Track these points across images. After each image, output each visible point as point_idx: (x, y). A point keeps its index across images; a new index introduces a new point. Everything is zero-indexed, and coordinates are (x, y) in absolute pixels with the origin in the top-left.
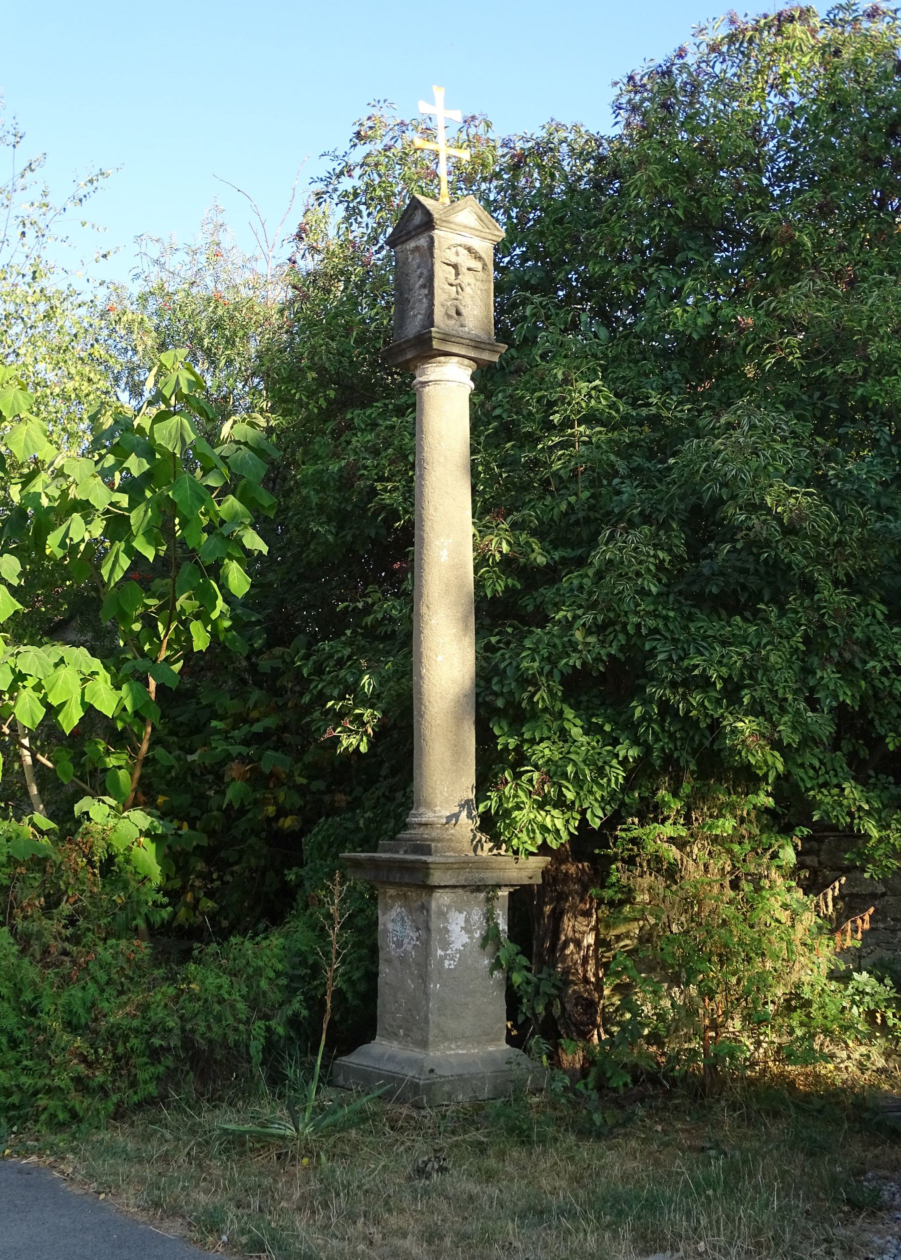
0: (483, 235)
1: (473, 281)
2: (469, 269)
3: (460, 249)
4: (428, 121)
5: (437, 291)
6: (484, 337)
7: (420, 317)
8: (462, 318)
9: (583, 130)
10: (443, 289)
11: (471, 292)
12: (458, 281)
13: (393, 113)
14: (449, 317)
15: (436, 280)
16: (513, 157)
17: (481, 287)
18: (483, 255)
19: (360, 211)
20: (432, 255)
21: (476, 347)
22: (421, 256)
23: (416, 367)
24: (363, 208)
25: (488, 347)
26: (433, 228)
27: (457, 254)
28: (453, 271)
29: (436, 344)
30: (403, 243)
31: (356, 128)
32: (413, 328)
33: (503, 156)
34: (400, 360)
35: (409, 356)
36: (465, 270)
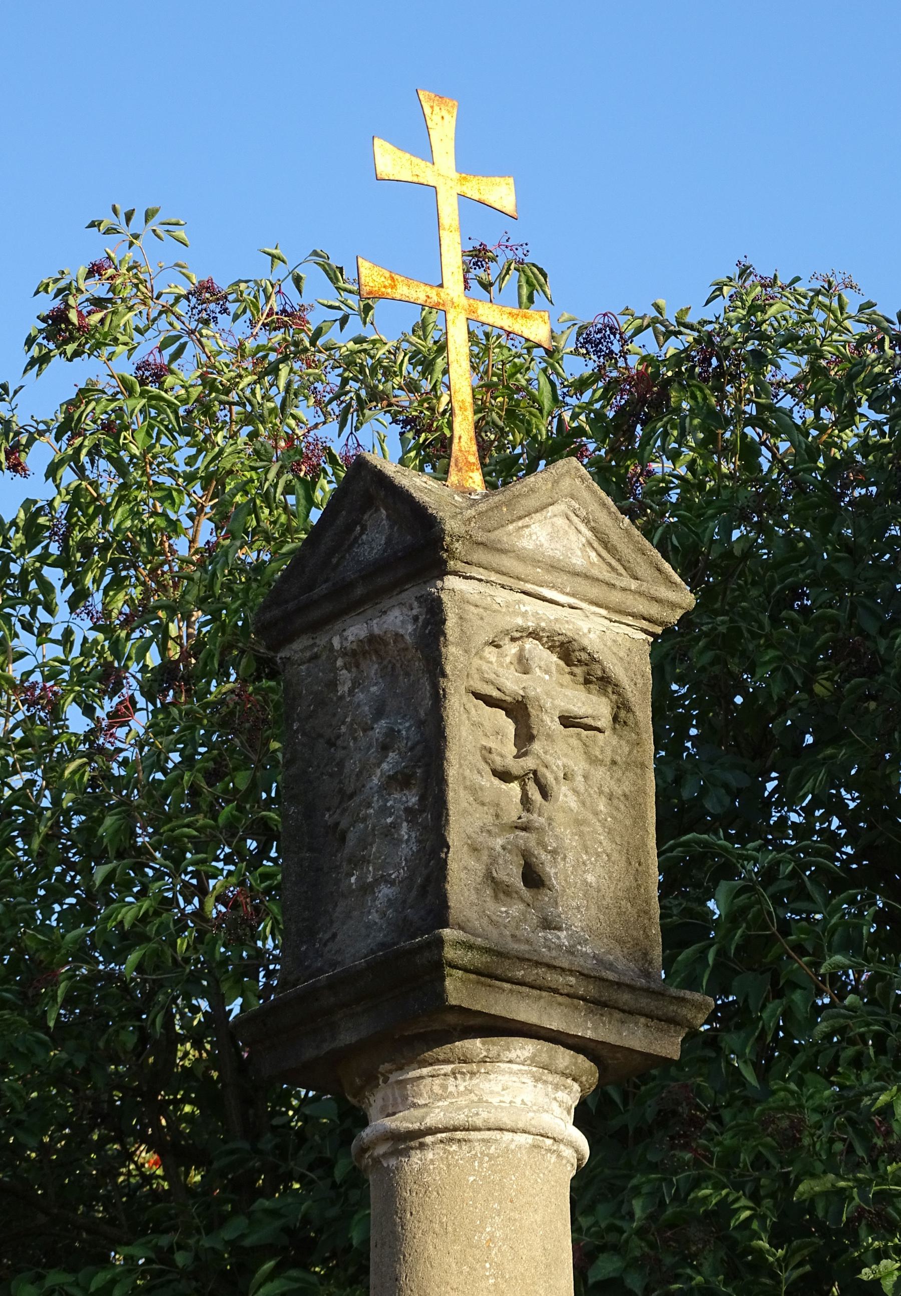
0: (615, 597)
1: (579, 766)
2: (567, 721)
3: (530, 644)
4: (289, 287)
5: (458, 799)
6: (624, 966)
7: (385, 892)
8: (545, 897)
9: (852, 303)
10: (474, 790)
11: (572, 802)
12: (529, 763)
13: (170, 252)
14: (500, 890)
15: (452, 755)
16: (612, 387)
17: (610, 785)
18: (618, 672)
19: (46, 587)
20: (435, 668)
21: (598, 1005)
22: (389, 673)
23: (371, 1080)
24: (54, 575)
25: (644, 1002)
26: (442, 571)
27: (523, 664)
28: (510, 727)
29: (457, 990)
30: (316, 627)
31: (48, 304)
32: (364, 925)
33: (581, 385)
34: (309, 1053)
35: (347, 1038)
36: (556, 726)
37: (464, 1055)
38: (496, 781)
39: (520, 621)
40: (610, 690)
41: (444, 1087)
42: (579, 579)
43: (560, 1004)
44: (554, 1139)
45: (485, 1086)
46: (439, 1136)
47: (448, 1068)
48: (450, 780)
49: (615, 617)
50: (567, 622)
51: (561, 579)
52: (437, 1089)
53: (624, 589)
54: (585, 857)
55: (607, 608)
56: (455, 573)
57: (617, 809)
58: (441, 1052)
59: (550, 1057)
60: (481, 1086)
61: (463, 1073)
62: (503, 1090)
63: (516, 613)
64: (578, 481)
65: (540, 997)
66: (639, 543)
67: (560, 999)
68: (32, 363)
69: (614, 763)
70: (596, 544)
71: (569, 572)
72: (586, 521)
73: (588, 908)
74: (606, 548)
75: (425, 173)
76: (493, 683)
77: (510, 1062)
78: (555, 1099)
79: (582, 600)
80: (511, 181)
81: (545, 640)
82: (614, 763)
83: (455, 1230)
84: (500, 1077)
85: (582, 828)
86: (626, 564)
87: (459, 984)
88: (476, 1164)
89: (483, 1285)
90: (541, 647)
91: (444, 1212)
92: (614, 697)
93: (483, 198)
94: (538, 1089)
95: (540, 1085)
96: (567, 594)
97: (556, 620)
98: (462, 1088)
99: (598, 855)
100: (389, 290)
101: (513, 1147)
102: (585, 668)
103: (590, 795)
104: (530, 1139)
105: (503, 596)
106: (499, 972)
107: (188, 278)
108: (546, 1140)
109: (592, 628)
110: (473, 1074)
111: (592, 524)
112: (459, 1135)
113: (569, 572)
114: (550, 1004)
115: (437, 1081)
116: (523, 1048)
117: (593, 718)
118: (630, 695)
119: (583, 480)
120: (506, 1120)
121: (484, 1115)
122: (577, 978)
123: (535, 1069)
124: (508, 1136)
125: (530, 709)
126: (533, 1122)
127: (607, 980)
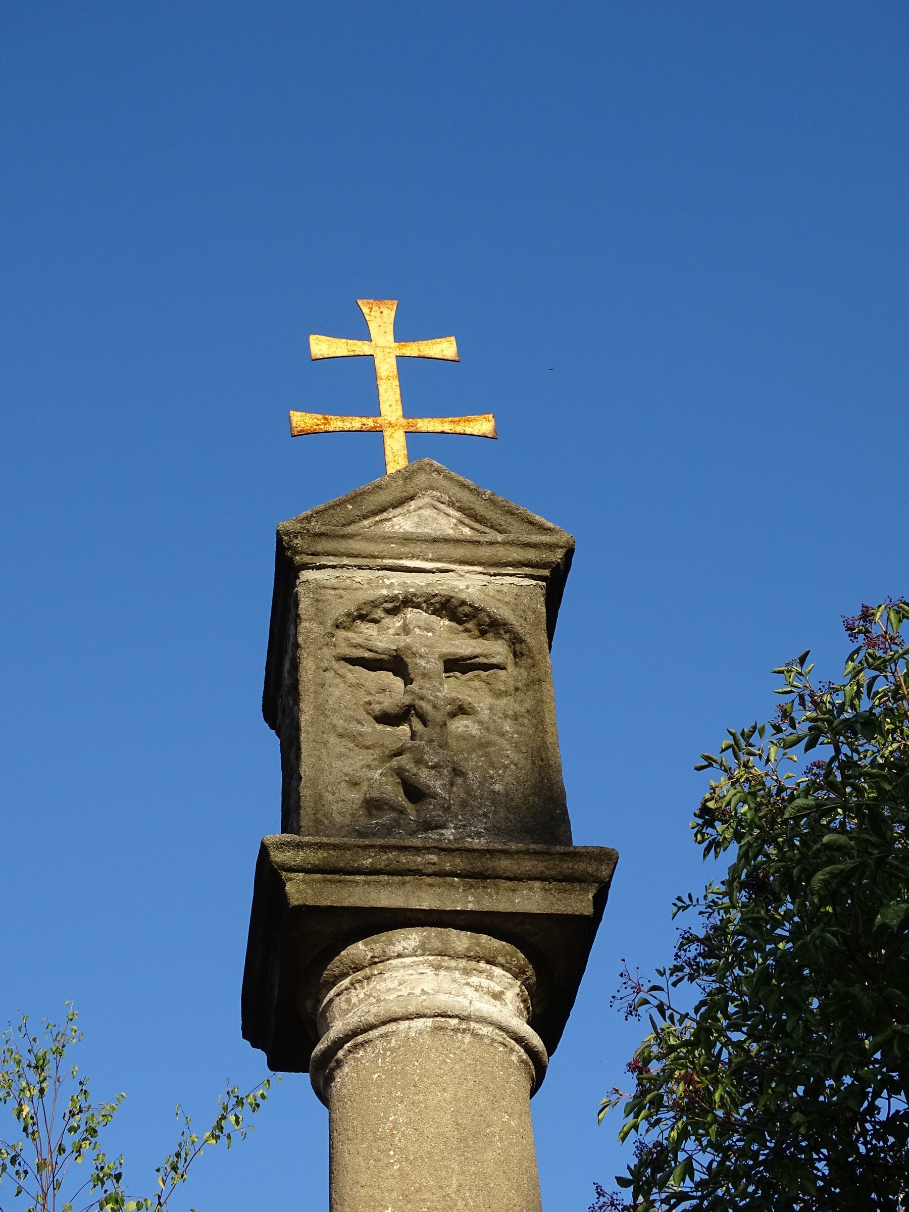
0: (485, 552)
18: (505, 613)
37: (353, 962)
38: (380, 727)
39: (385, 592)
40: (502, 632)
41: (348, 1001)
42: (440, 545)
43: (431, 885)
44: (460, 1018)
45: (382, 986)
46: (346, 1046)
47: (346, 982)
48: (303, 724)
49: (492, 571)
50: (441, 584)
51: (417, 549)
52: (344, 1006)
53: (491, 543)
54: (491, 772)
55: (480, 564)
56: (306, 566)
57: (522, 725)
58: (334, 967)
59: (442, 941)
60: (378, 987)
61: (359, 981)
62: (400, 985)
63: (379, 587)
64: (434, 475)
65: (404, 883)
66: (504, 506)
67: (428, 880)
68: (707, 850)
69: (517, 689)
70: (467, 521)
71: (426, 541)
72: (451, 504)
73: (495, 813)
74: (477, 521)
75: (361, 348)
76: (361, 646)
77: (399, 956)
78: (468, 984)
79: (450, 562)
80: (453, 339)
81: (424, 605)
82: (517, 689)
83: (363, 1129)
84: (394, 974)
85: (487, 750)
86: (499, 528)
87: (302, 886)
88: (380, 1061)
89: (388, 1172)
90: (424, 614)
91: (355, 1116)
92: (507, 636)
93: (422, 354)
94: (440, 977)
95: (442, 973)
96: (432, 560)
97: (428, 585)
98: (362, 996)
99: (506, 767)
100: (322, 427)
101: (413, 1034)
102: (474, 621)
103: (494, 721)
104: (429, 1022)
105: (361, 576)
106: (342, 864)
107: (791, 759)
108: (450, 1020)
109: (468, 584)
110: (368, 978)
111: (458, 504)
112: (360, 1038)
113: (426, 541)
114: (419, 887)
115: (343, 998)
116: (406, 938)
117: (485, 656)
118: (519, 629)
119: (438, 471)
120: (399, 1011)
121: (374, 1010)
122: (438, 855)
123: (431, 958)
124: (404, 1025)
125: (406, 659)
126: (425, 1004)
127: (474, 850)
